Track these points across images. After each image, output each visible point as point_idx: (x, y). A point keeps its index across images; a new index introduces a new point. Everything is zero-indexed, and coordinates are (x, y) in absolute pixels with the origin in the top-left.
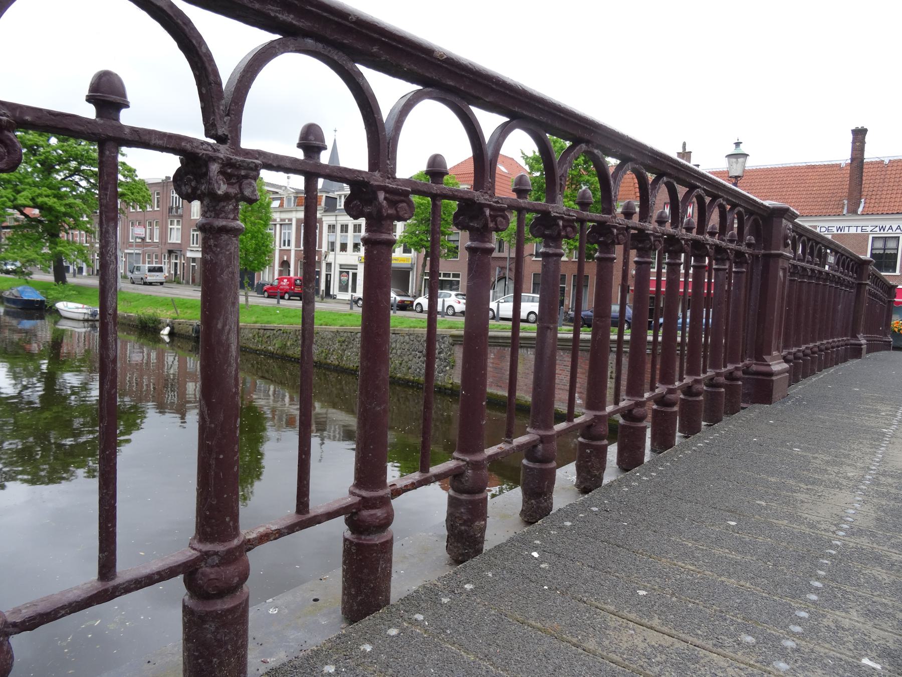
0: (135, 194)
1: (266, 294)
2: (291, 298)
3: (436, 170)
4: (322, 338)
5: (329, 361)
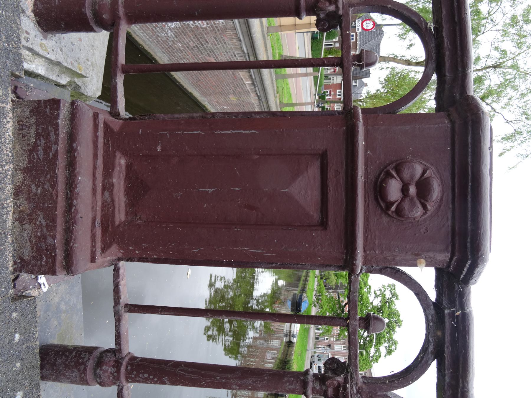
0: (363, 362)
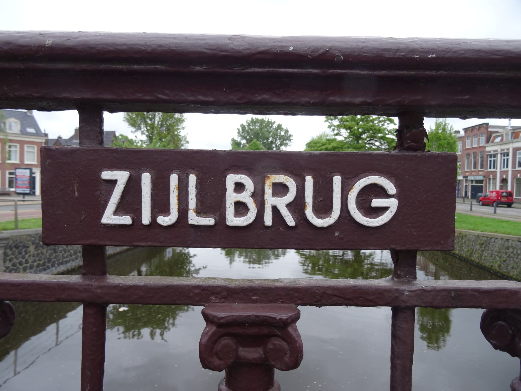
1: (481, 203)
2: (499, 205)
3: (341, 130)
4: (468, 240)
5: (473, 259)
